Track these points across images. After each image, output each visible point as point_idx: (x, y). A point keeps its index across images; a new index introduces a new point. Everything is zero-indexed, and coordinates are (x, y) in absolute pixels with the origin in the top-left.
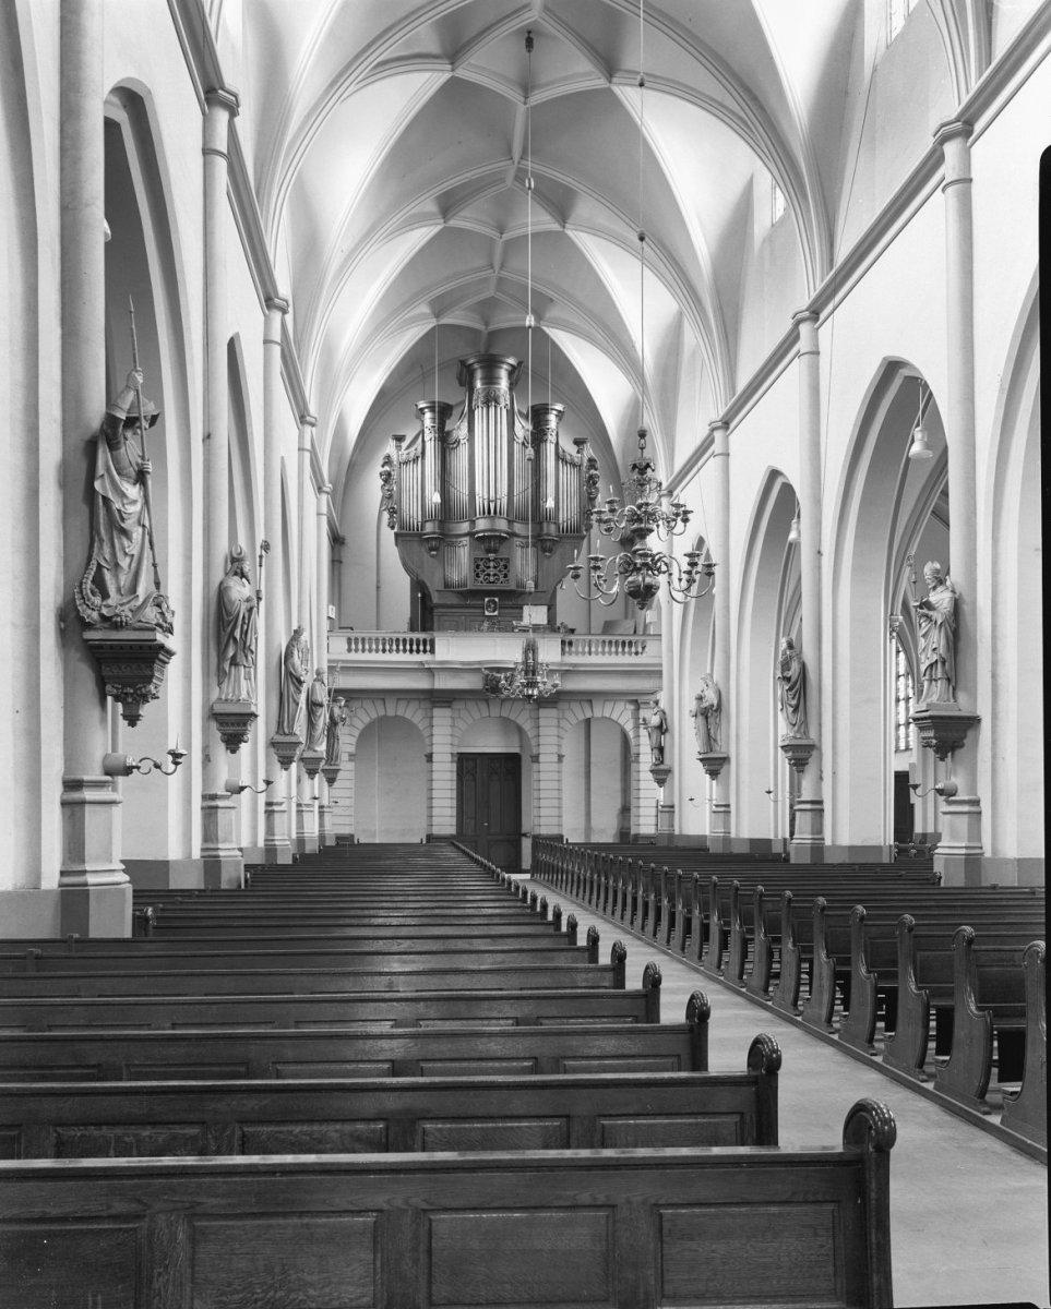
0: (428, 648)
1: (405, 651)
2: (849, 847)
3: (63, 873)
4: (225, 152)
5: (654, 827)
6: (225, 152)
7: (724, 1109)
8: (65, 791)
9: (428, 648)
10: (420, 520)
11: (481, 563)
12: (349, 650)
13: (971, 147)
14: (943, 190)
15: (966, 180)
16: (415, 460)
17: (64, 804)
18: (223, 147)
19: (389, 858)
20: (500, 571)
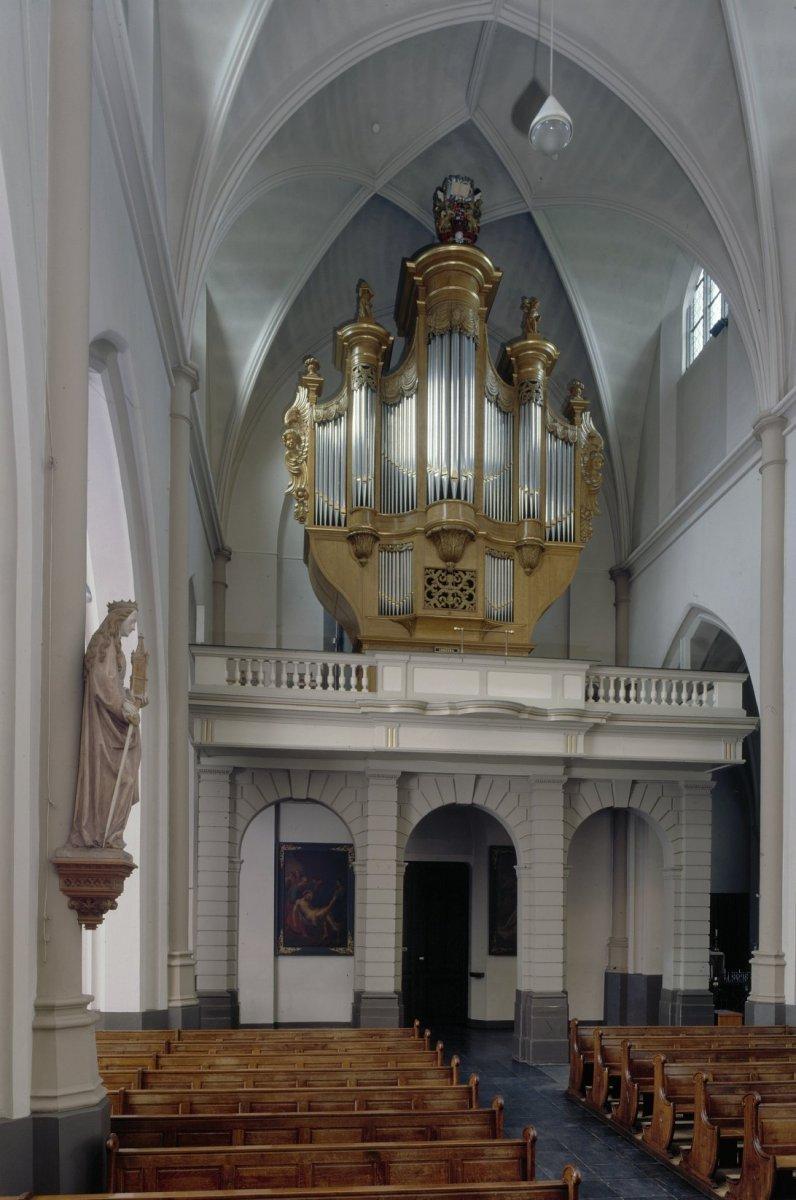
0: (365, 681)
1: (325, 685)
2: (58, 1193)
3: (33, 1098)
4: (188, 416)
5: (561, 981)
6: (188, 416)
7: (283, 997)
8: (37, 1015)
9: (365, 681)
10: (343, 510)
11: (435, 576)
12: (231, 681)
13: (787, 434)
14: (761, 471)
15: (782, 462)
16: (336, 419)
17: (35, 1029)
18: (186, 413)
19: (484, 1113)
20: (462, 590)
